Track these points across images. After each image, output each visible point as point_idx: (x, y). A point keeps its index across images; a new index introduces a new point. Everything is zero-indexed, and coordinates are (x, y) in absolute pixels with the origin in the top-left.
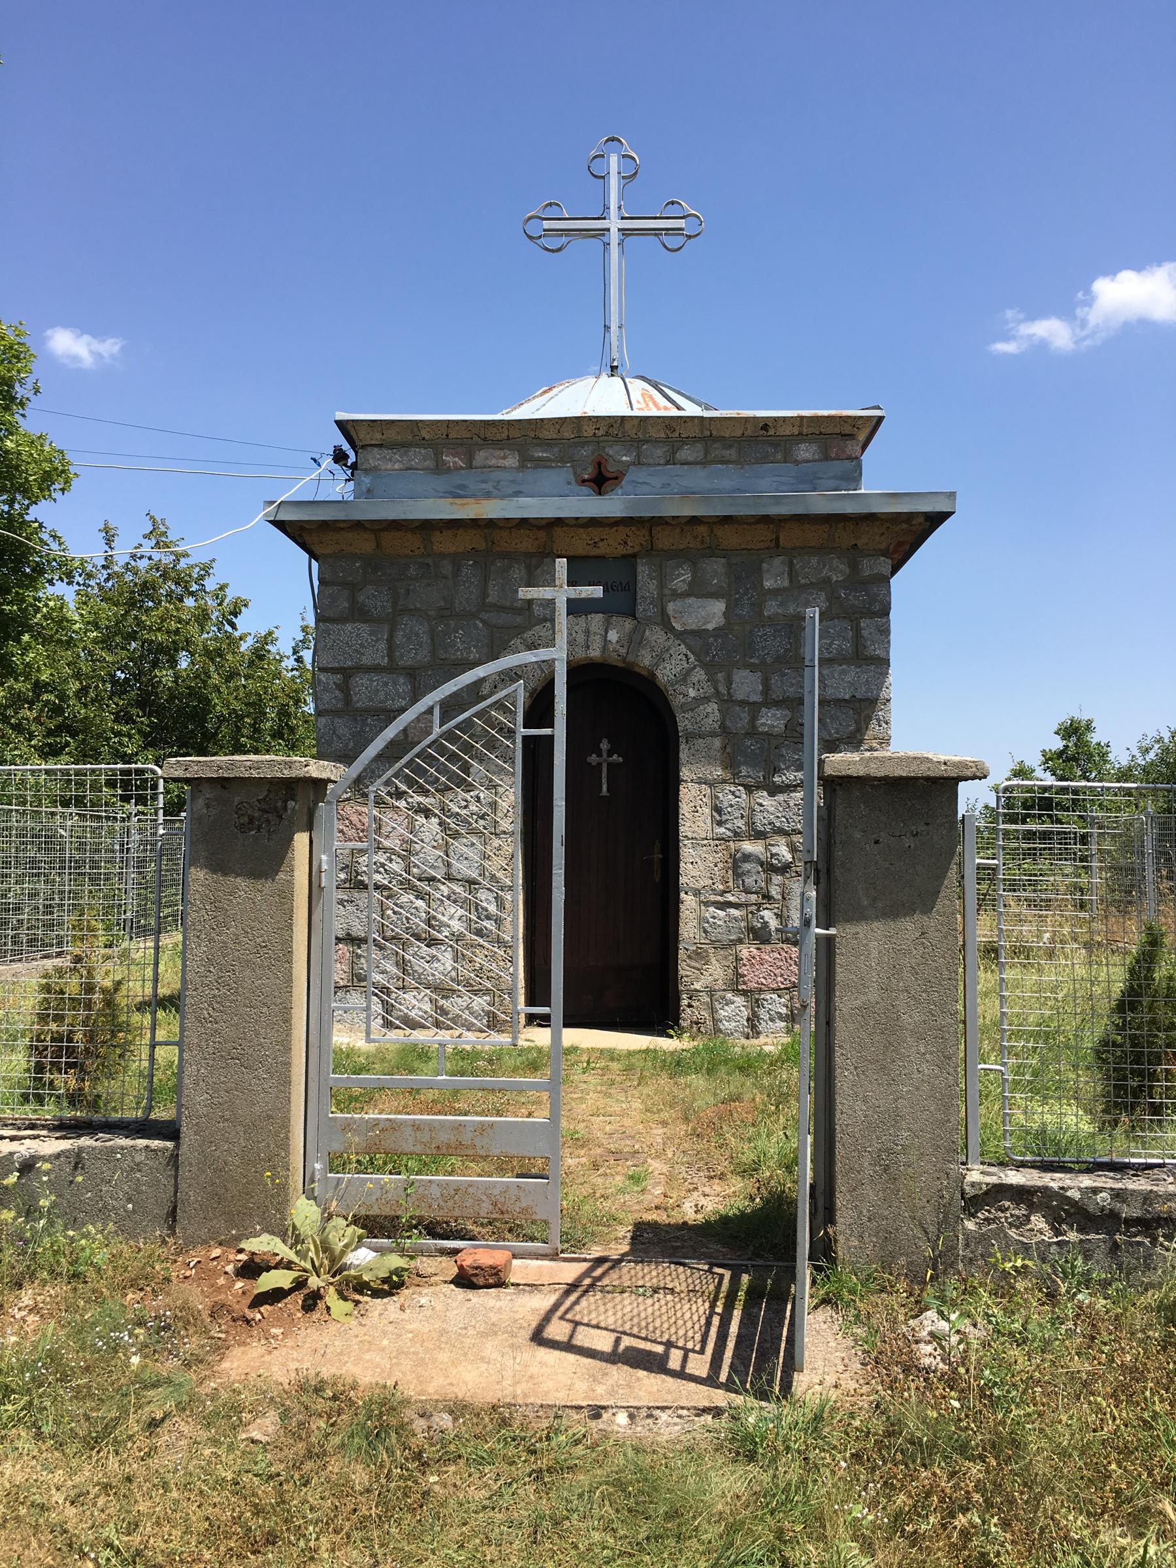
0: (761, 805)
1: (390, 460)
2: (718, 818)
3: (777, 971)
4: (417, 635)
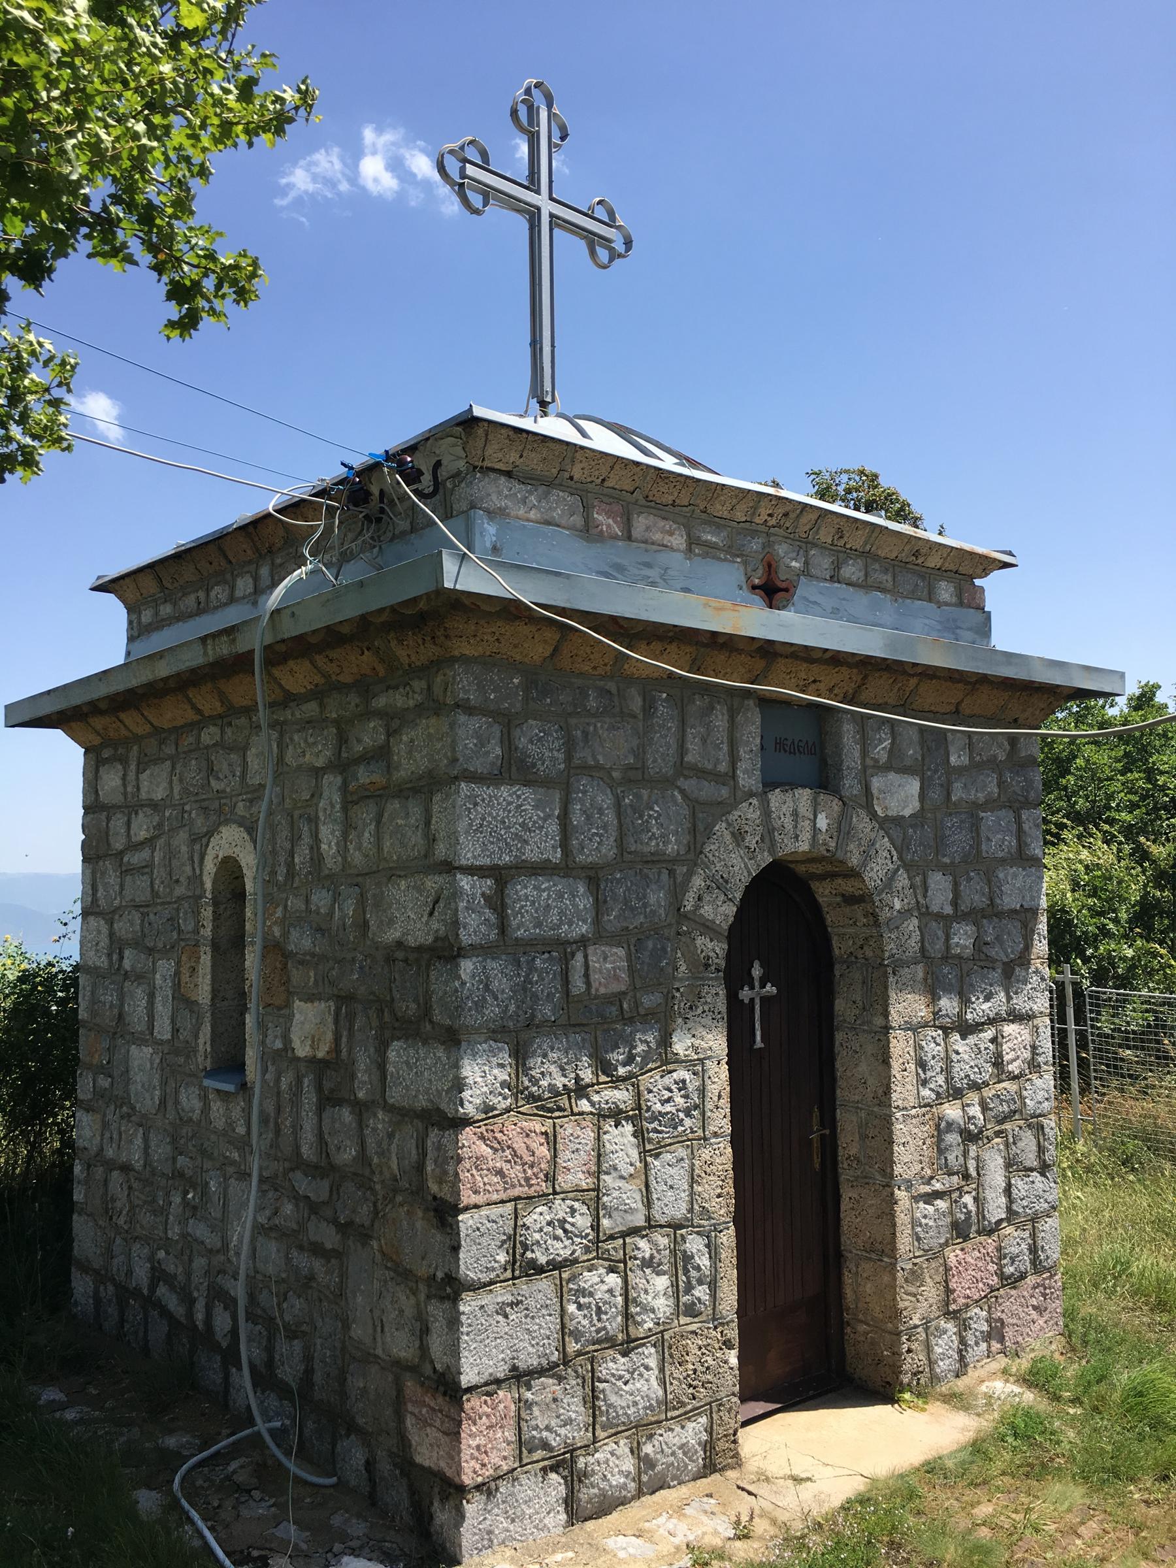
1: (524, 501)
2: (923, 1076)
4: (601, 811)
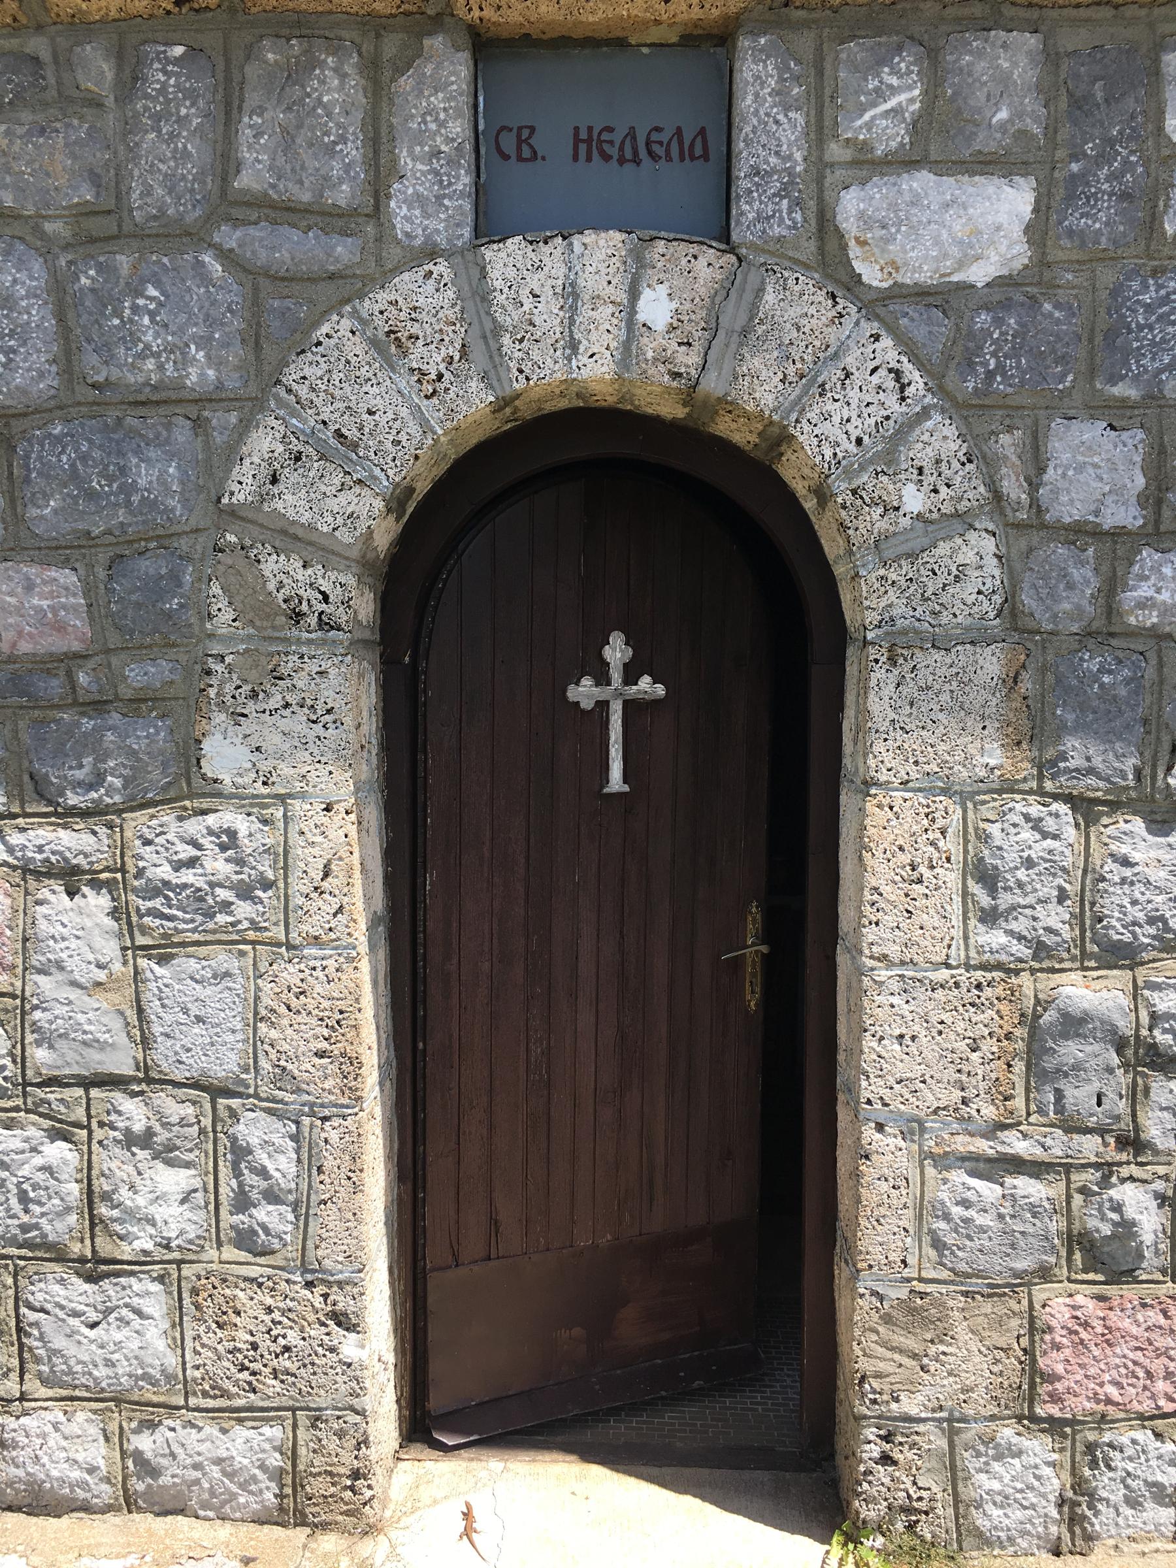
0: (1126, 862)
2: (985, 900)
3: (1157, 1366)
